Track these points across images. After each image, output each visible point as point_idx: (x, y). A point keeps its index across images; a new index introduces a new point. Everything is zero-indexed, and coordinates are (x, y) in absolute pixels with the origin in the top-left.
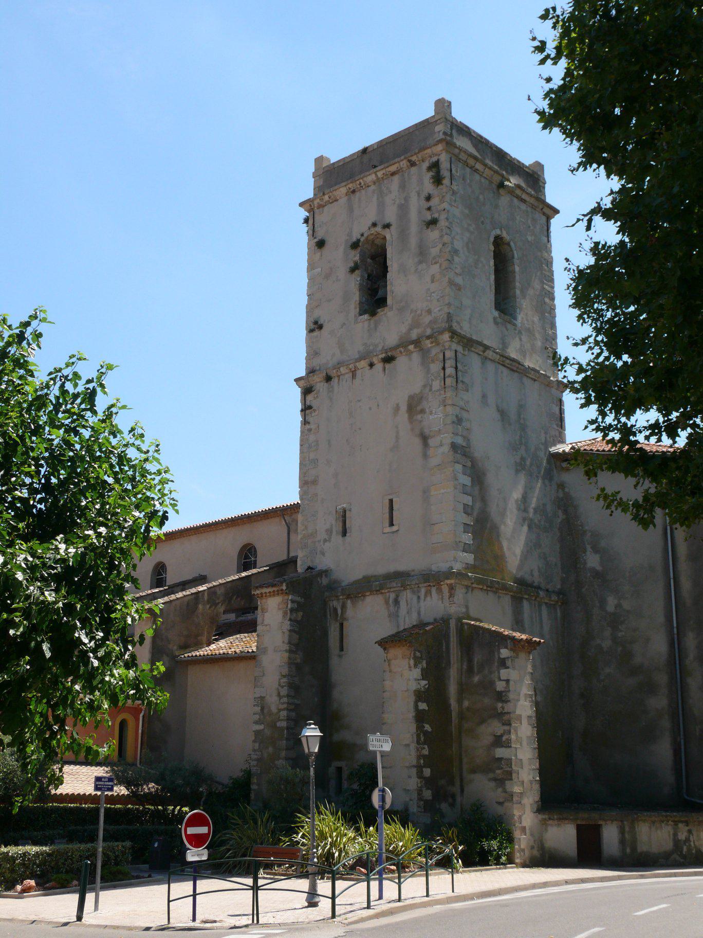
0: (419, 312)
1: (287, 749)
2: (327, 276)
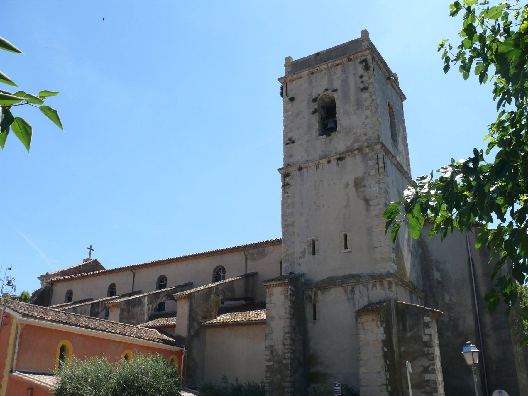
0: (358, 134)
1: (290, 376)
2: (297, 116)
